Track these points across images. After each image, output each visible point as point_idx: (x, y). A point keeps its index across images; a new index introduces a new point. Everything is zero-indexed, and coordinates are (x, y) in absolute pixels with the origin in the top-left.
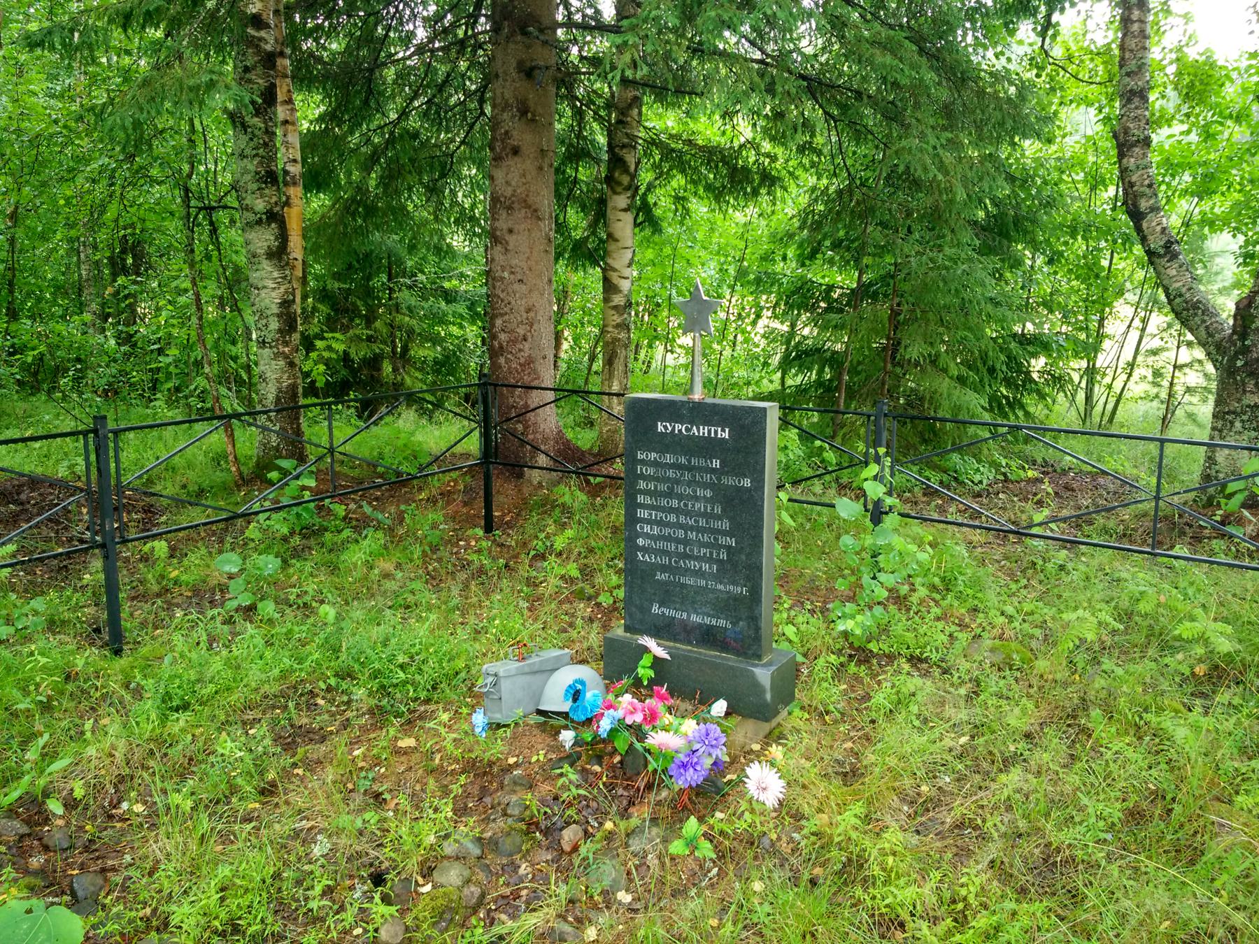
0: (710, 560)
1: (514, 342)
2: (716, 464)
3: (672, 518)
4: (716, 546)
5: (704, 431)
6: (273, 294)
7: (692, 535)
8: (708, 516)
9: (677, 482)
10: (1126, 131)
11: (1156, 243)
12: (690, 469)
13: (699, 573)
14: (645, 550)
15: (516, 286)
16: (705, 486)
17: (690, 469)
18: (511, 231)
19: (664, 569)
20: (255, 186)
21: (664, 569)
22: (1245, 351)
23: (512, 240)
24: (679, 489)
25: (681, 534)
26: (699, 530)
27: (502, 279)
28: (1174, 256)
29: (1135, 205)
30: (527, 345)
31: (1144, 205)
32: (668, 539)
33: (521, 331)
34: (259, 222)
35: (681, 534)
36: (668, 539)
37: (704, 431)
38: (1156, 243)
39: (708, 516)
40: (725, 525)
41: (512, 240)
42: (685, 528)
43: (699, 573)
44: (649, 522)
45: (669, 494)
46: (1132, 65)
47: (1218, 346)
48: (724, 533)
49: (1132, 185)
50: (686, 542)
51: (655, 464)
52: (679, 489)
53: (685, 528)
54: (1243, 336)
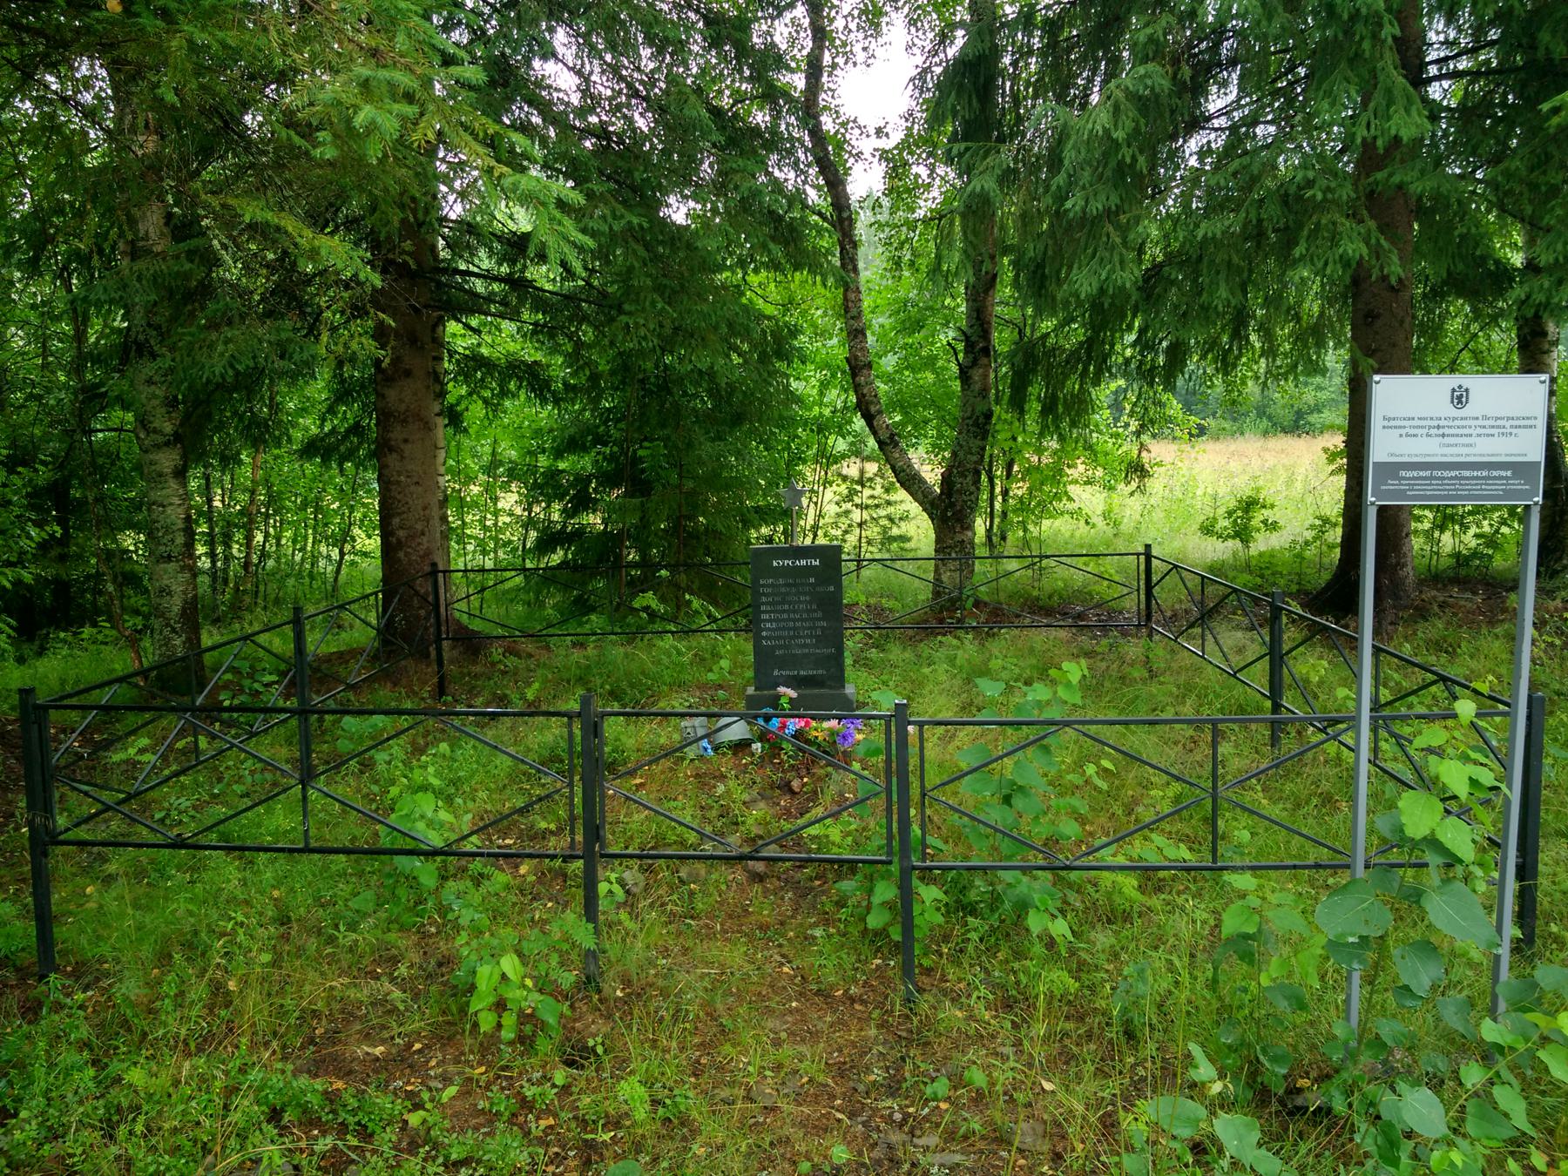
0: (811, 637)
1: (412, 537)
2: (812, 580)
3: (785, 616)
4: (815, 628)
5: (803, 562)
6: (180, 510)
7: (798, 624)
8: (808, 611)
9: (787, 594)
10: (856, 358)
11: (884, 436)
12: (795, 585)
13: (805, 646)
14: (766, 638)
15: (413, 488)
16: (805, 594)
17: (795, 585)
18: (406, 441)
19: (780, 647)
20: (163, 410)
21: (780, 647)
22: (952, 505)
23: (407, 448)
24: (789, 598)
25: (791, 624)
26: (802, 620)
27: (398, 483)
28: (896, 445)
29: (868, 410)
30: (425, 539)
31: (873, 409)
32: (784, 629)
33: (419, 527)
34: (167, 444)
35: (791, 624)
36: (784, 629)
37: (803, 562)
38: (884, 436)
39: (808, 611)
40: (820, 614)
41: (407, 448)
42: (794, 620)
43: (805, 646)
44: (770, 621)
45: (783, 602)
46: (854, 312)
47: (932, 504)
48: (819, 619)
49: (864, 395)
50: (795, 629)
51: (772, 585)
52: (789, 598)
53: (794, 620)
54: (949, 496)
